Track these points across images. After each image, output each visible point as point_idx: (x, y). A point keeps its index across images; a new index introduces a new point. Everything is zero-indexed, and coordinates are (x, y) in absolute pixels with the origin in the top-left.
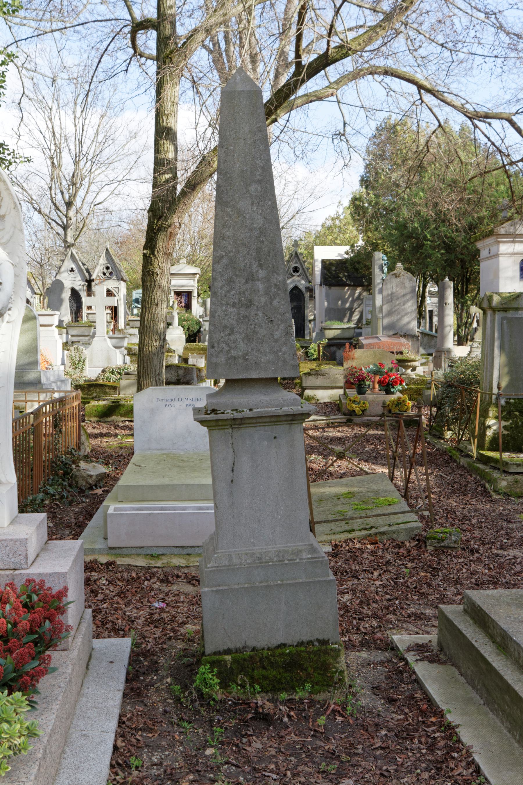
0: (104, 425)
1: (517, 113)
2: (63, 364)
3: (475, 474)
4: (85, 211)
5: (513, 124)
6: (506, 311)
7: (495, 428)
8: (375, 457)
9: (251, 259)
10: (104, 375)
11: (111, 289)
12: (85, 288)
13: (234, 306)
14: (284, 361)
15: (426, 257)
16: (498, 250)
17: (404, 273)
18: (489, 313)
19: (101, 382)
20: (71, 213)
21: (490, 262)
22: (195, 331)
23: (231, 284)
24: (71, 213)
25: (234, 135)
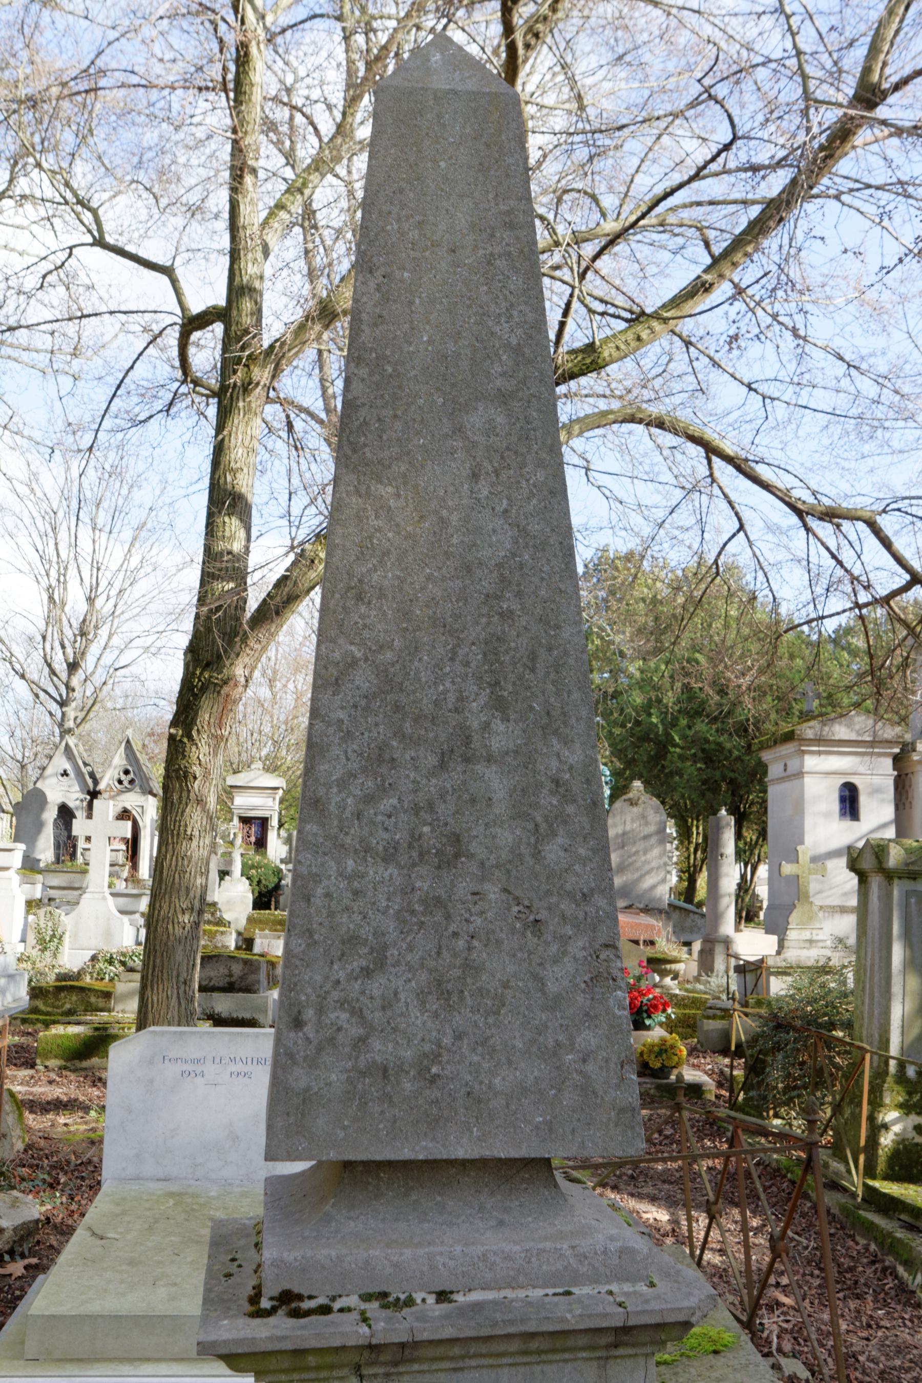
0: (72, 1077)
1: (884, 511)
2: (23, 940)
3: (863, 1236)
4: (98, 679)
5: (877, 531)
6: (915, 879)
7: (897, 1128)
8: (632, 1177)
9: (465, 677)
10: (93, 966)
11: (129, 808)
12: (85, 804)
13: (389, 856)
14: (586, 1089)
15: (671, 775)
16: (802, 766)
17: (645, 797)
18: (876, 882)
19: (87, 980)
20: (75, 682)
21: (786, 785)
22: (271, 886)
23: (384, 770)
24: (75, 682)
25: (414, 234)
